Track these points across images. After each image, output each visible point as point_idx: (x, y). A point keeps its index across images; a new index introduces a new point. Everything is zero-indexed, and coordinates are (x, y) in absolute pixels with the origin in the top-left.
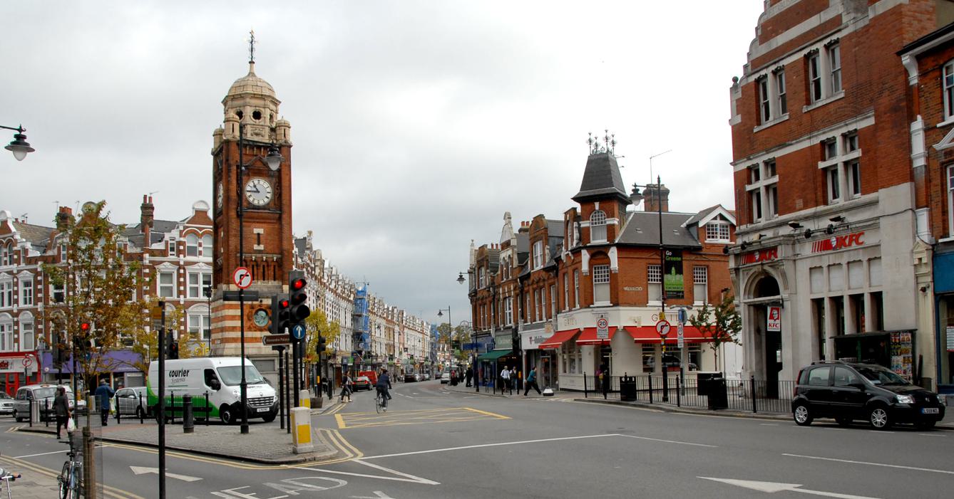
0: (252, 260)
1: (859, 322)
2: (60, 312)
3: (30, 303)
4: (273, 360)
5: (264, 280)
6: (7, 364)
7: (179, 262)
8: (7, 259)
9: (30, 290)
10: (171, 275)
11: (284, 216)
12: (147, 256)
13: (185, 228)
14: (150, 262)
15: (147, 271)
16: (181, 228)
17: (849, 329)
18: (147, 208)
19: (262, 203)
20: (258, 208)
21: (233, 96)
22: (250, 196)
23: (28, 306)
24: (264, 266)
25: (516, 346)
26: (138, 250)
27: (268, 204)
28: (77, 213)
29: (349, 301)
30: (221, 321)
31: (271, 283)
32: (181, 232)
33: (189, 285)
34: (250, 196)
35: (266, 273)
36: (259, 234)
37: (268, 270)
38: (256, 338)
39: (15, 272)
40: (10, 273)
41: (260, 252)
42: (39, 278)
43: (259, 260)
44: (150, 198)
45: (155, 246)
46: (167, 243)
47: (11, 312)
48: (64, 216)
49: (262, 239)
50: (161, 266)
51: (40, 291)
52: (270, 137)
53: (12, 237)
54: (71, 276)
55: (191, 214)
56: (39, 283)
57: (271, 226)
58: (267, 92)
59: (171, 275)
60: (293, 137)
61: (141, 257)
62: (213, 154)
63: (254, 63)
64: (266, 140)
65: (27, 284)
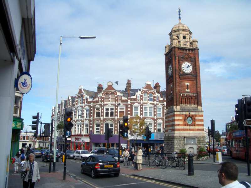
0: (189, 96)
1: (181, 120)
2: (98, 121)
3: (97, 132)
4: (195, 139)
5: (186, 104)
6: (79, 139)
7: (141, 103)
8: (81, 102)
9: (88, 113)
10: (138, 107)
11: (198, 77)
12: (129, 101)
13: (143, 90)
14: (131, 103)
15: (129, 106)
16: (142, 90)
17: (181, 123)
18: (129, 84)
19: (188, 72)
20: (187, 74)
21: (174, 31)
22: (184, 69)
23: (87, 118)
24: (190, 99)
25: (177, 130)
26: (126, 99)
27: (191, 73)
28: (105, 87)
29: (41, 134)
30: (172, 122)
31: (193, 106)
32: (142, 92)
33: (144, 111)
34: (184, 69)
35: (191, 101)
36: (187, 85)
37: (192, 100)
38: (188, 129)
39: (83, 106)
40: (82, 107)
41: (188, 92)
42: (91, 108)
43: (188, 96)
44: (130, 80)
45: (132, 97)
46: (136, 96)
47: (81, 120)
48: (100, 88)
49: (189, 87)
50: (135, 104)
51: (91, 113)
52: (190, 46)
53: (83, 94)
54: (102, 108)
55: (145, 86)
56: (91, 110)
57: (192, 82)
58: (187, 29)
59: (138, 107)
60: (199, 46)
61: (127, 101)
62: (166, 55)
63: (180, 19)
64: (189, 47)
65: (87, 110)
